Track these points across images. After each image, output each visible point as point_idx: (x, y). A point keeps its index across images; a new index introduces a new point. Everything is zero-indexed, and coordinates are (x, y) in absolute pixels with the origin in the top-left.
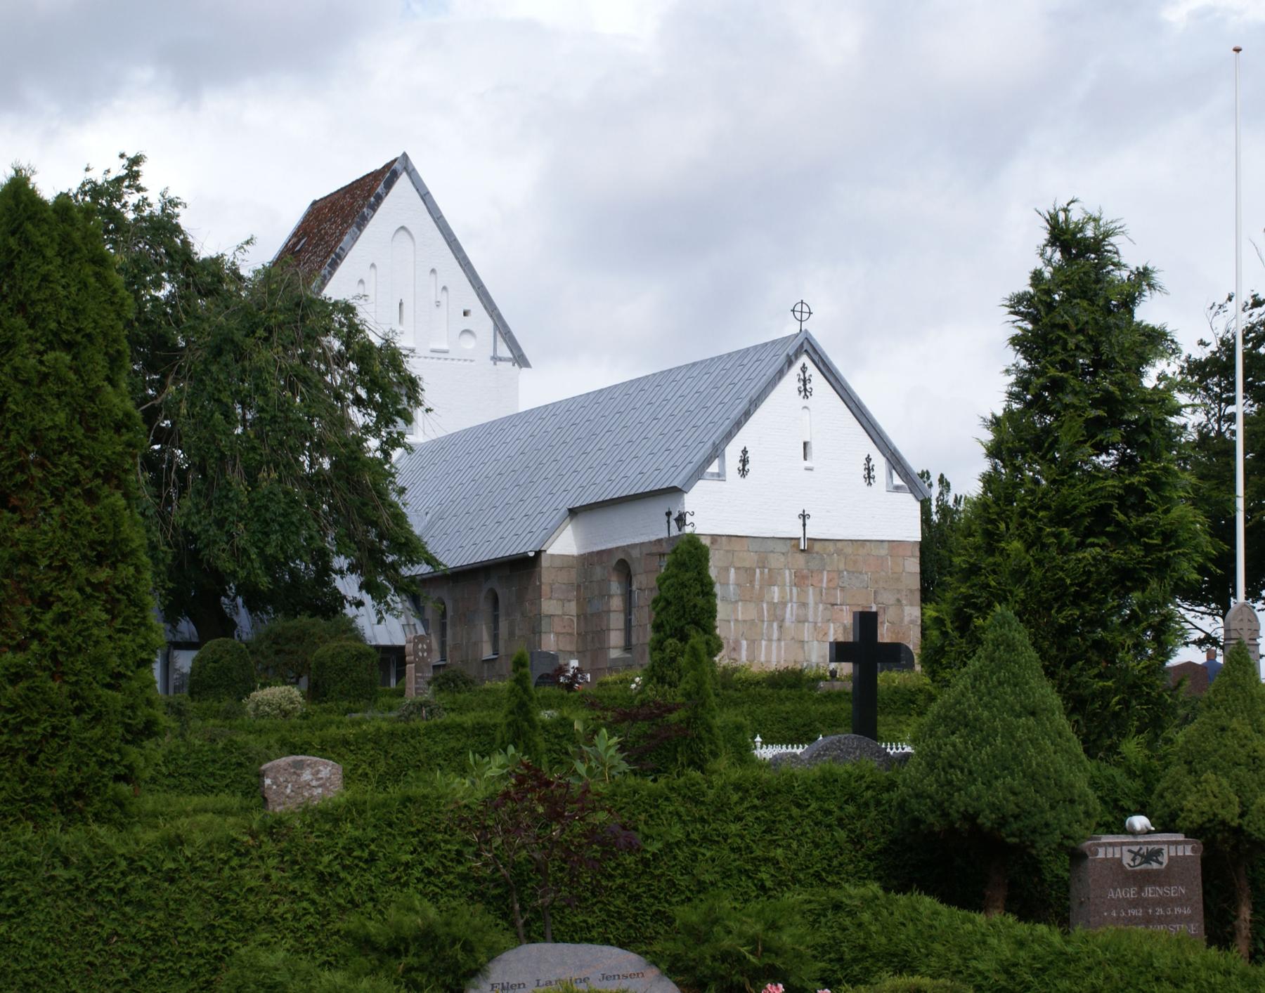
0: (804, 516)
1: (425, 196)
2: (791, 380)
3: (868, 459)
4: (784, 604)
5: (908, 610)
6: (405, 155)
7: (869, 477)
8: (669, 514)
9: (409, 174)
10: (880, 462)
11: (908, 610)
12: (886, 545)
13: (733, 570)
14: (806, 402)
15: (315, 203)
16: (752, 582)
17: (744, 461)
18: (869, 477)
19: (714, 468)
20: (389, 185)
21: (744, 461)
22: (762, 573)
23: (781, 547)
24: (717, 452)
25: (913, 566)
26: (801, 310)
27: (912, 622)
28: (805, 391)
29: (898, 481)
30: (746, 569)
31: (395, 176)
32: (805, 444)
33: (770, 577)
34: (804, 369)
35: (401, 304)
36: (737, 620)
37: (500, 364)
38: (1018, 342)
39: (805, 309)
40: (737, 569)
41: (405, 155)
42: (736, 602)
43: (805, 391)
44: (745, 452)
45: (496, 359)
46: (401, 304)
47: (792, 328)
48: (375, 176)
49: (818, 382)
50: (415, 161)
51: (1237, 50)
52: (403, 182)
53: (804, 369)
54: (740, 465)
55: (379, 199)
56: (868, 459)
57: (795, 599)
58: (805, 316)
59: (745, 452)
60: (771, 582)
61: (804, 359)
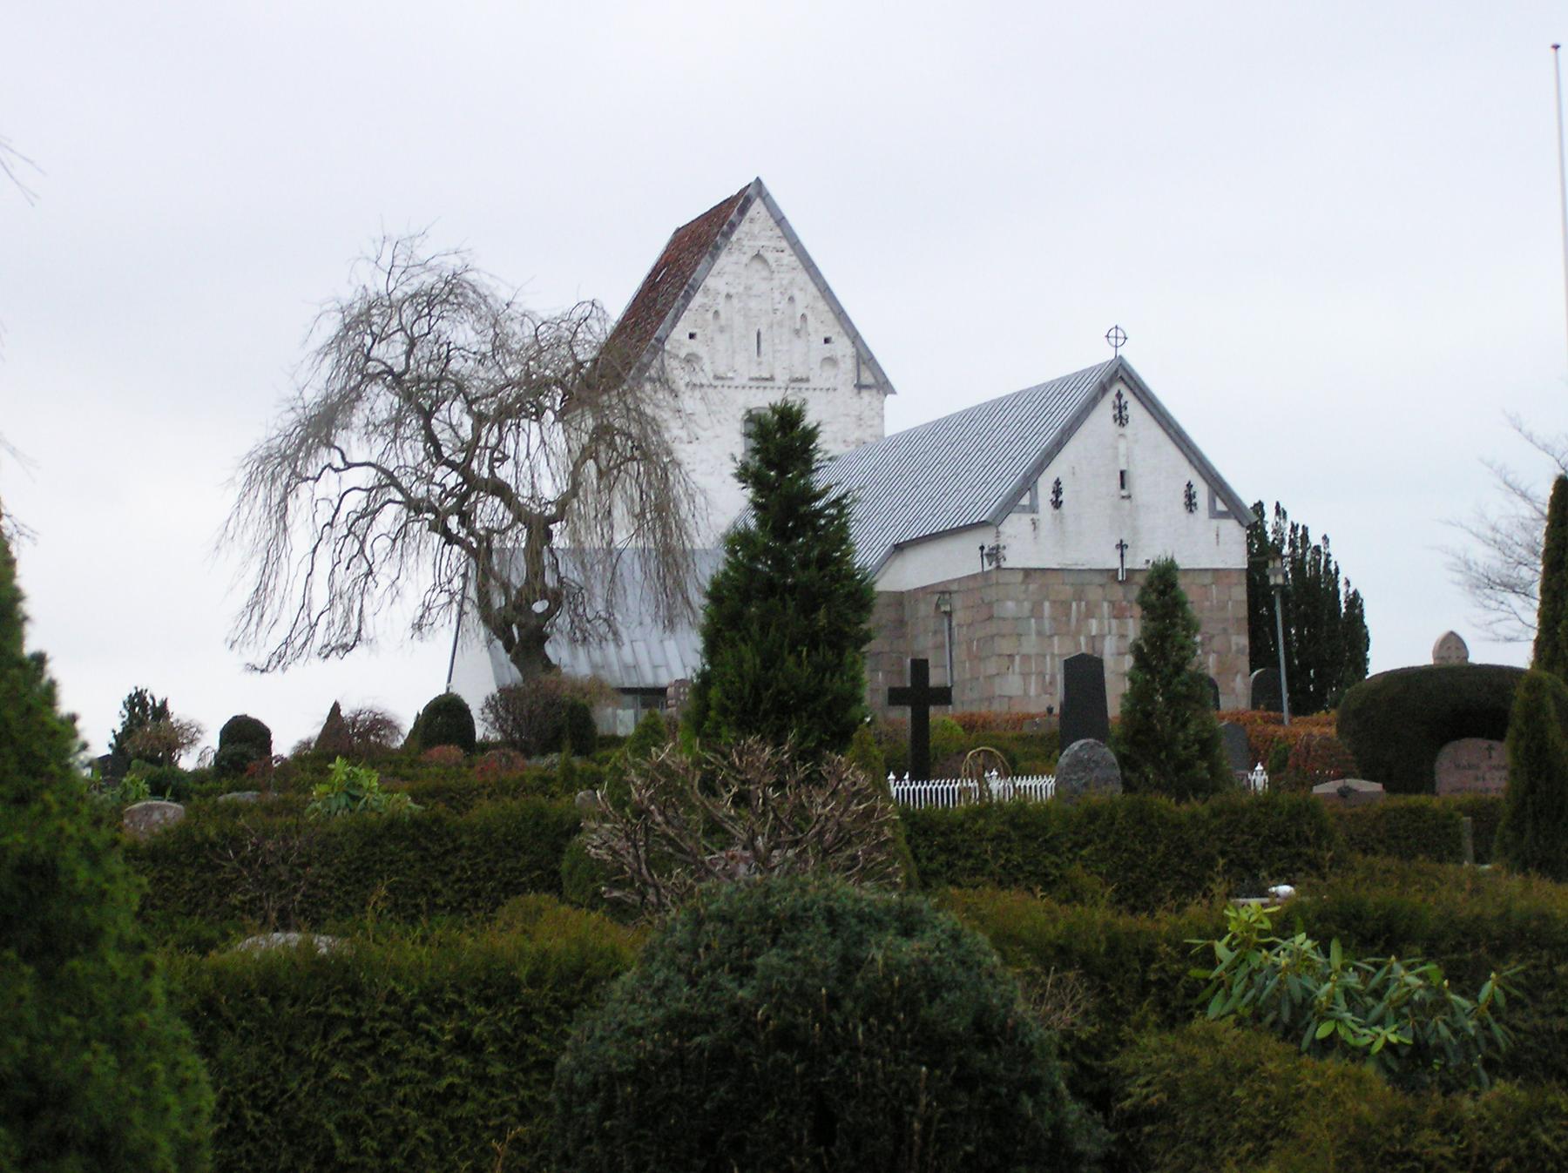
0: (1122, 546)
1: (781, 221)
2: (1106, 409)
3: (1189, 486)
4: (1103, 637)
5: (1234, 639)
6: (758, 180)
7: (1190, 503)
8: (982, 548)
9: (764, 199)
10: (1202, 491)
11: (1234, 639)
12: (1209, 574)
13: (1047, 604)
14: (1121, 430)
15: (678, 230)
16: (1068, 615)
17: (1057, 491)
18: (1190, 503)
19: (1025, 501)
20: (743, 211)
21: (1057, 491)
22: (1079, 606)
23: (1098, 579)
24: (1028, 483)
25: (1240, 593)
26: (1116, 335)
27: (1239, 651)
28: (1121, 419)
29: (1221, 506)
30: (1063, 602)
31: (748, 201)
32: (1122, 473)
33: (1088, 609)
34: (1119, 396)
35: (759, 335)
36: (1053, 655)
37: (865, 394)
38: (748, 435)
39: (1120, 334)
40: (1053, 602)
41: (758, 180)
42: (1051, 636)
43: (1121, 419)
44: (1058, 483)
45: (860, 387)
46: (759, 335)
47: (1105, 355)
48: (729, 203)
49: (1135, 409)
50: (769, 186)
51: (1556, 47)
52: (757, 208)
53: (1119, 396)
54: (1053, 497)
55: (733, 226)
56: (1189, 486)
57: (1114, 631)
58: (1120, 341)
59: (1058, 483)
60: (1090, 614)
61: (1120, 386)
